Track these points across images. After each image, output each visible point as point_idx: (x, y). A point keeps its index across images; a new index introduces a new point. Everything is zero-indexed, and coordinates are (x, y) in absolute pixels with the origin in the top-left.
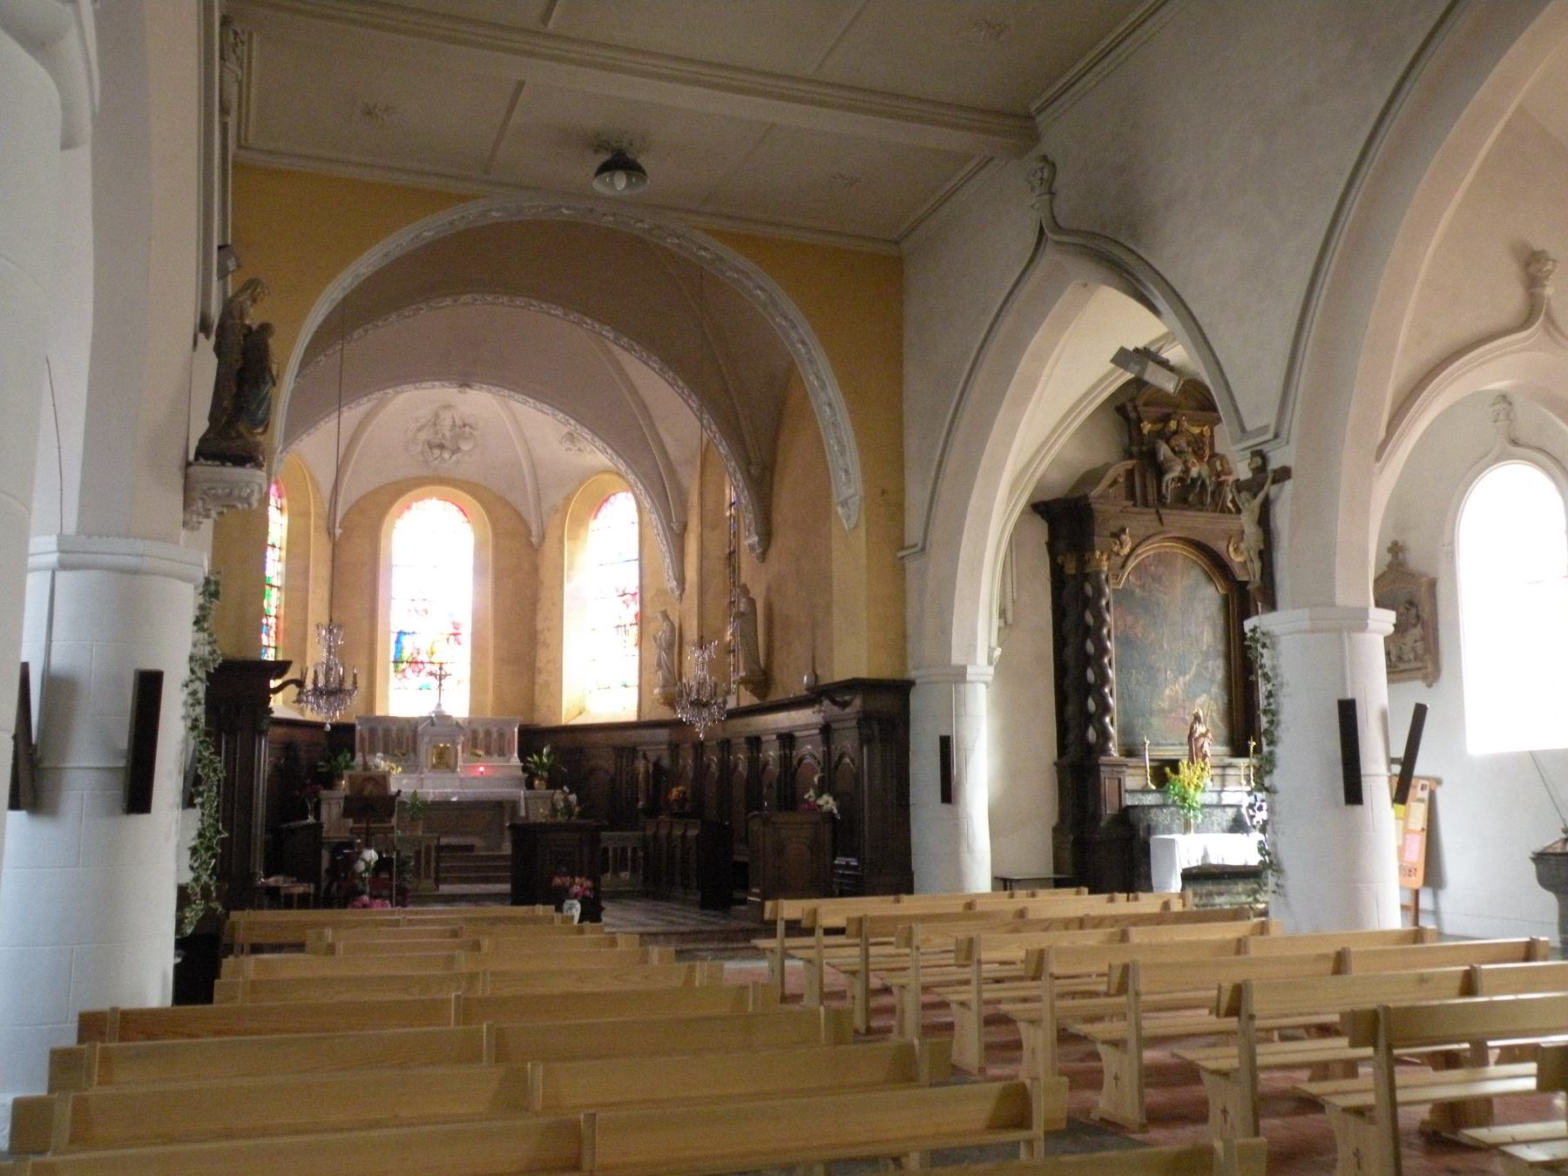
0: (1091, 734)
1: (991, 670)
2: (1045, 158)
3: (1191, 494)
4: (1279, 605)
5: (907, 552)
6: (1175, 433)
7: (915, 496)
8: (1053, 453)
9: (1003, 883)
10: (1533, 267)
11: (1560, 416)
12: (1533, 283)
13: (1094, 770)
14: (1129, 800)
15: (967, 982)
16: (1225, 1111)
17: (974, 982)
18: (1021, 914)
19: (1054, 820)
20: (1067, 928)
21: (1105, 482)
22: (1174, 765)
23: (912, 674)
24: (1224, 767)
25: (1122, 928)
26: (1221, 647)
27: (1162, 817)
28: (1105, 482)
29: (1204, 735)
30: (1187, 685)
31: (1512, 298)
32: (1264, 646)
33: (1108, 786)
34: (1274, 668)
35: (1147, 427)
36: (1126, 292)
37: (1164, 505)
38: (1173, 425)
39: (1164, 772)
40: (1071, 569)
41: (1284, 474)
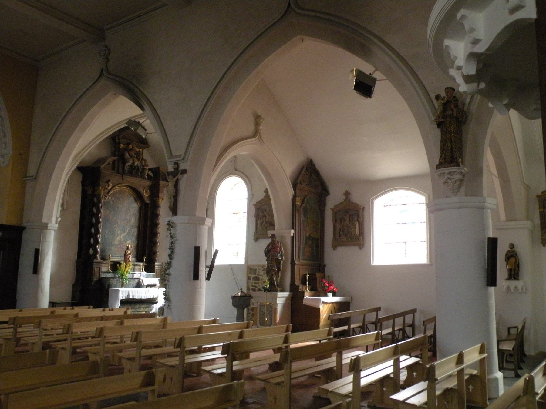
0: (91, 251)
1: (57, 226)
2: (106, 46)
3: (134, 171)
4: (178, 214)
5: (27, 179)
6: (131, 149)
7: (34, 158)
8: (89, 150)
9: (52, 304)
10: (257, 119)
11: (258, 165)
12: (257, 124)
13: (92, 264)
14: (103, 275)
15: (65, 340)
16: (172, 379)
17: (69, 340)
18: (76, 315)
19: (73, 282)
20: (97, 321)
21: (106, 163)
22: (120, 264)
23: (25, 225)
24: (134, 265)
25: (15, 322)
26: (137, 225)
27: (114, 282)
28: (106, 163)
29: (130, 254)
30: (125, 236)
31: (251, 128)
32: (172, 227)
33: (96, 270)
34: (174, 234)
35: (122, 146)
36: (132, 100)
37: (124, 174)
38: (130, 147)
39: (115, 266)
40: (90, 192)
41: (184, 172)
